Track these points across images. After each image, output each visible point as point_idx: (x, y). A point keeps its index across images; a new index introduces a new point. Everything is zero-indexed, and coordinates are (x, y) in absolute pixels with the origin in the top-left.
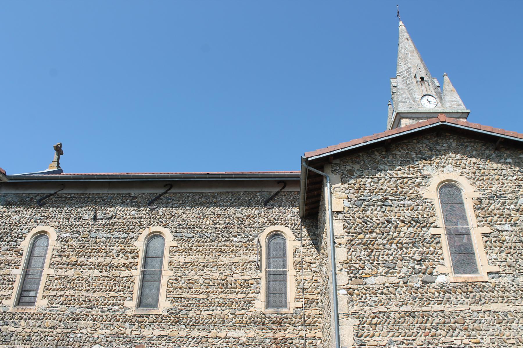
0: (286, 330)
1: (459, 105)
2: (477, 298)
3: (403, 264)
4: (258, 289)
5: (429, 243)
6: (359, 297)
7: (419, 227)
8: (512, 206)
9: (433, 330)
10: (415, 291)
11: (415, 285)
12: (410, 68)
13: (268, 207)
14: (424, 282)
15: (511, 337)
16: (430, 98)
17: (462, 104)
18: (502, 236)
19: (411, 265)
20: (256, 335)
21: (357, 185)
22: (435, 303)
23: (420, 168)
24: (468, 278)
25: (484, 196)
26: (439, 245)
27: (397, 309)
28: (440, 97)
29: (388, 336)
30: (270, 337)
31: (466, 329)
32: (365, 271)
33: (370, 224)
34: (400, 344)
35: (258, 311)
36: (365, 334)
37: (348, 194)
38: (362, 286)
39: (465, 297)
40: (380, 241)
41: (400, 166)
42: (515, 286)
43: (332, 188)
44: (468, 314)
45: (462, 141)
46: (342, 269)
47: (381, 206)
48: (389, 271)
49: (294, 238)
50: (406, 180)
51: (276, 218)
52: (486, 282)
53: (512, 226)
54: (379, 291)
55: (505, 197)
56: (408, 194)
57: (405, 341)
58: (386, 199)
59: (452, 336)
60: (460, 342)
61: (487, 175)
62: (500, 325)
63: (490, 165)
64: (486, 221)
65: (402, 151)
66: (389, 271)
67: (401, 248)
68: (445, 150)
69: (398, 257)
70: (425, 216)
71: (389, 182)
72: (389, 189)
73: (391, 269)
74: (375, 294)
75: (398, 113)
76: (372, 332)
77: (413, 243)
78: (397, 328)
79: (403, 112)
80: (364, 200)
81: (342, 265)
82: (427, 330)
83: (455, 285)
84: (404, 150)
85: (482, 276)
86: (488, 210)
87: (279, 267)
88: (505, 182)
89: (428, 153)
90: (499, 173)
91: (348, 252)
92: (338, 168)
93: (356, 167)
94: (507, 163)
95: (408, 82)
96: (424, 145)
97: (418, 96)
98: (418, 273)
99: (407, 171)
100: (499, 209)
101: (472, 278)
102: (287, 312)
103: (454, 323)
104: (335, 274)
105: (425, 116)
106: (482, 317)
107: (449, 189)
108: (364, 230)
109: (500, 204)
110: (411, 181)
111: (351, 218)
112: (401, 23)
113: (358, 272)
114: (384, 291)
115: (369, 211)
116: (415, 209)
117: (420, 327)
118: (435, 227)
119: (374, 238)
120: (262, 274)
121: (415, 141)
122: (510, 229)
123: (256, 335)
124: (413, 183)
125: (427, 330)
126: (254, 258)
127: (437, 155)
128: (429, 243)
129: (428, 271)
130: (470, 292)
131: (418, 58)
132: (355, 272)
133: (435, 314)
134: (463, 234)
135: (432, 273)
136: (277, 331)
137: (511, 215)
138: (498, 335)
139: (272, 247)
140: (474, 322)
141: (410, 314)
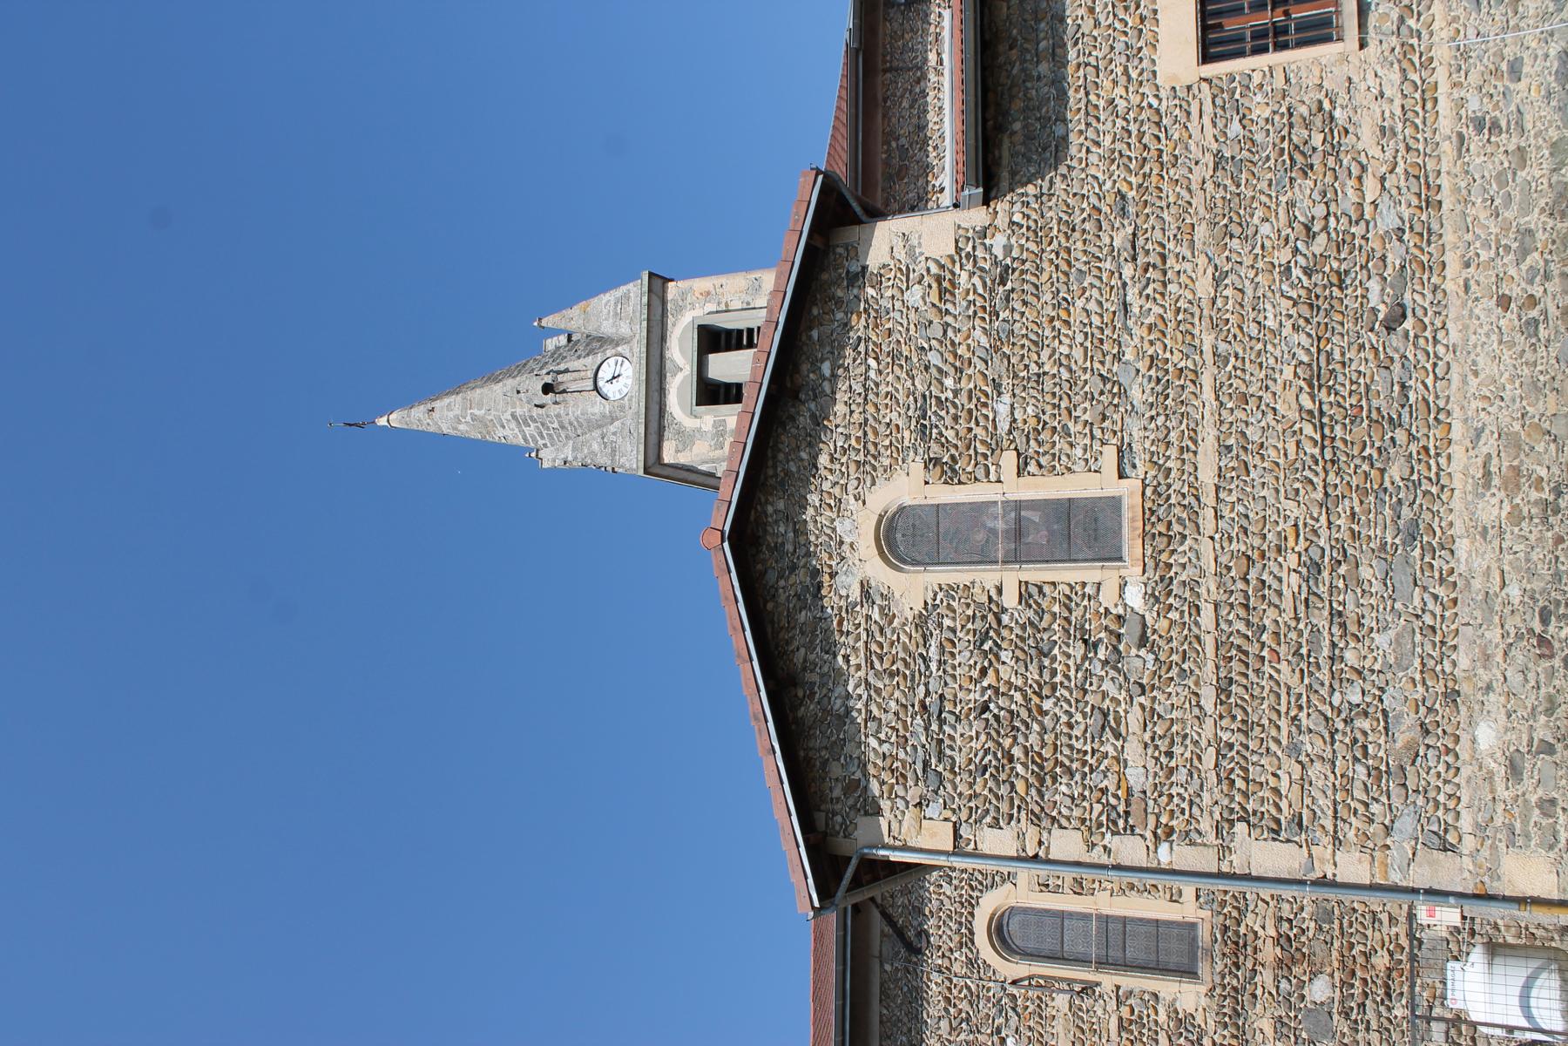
0: (1256, 933)
1: (627, 297)
2: (1185, 515)
3: (1094, 688)
4: (1146, 997)
5: (1040, 613)
6: (1177, 814)
7: (998, 634)
8: (949, 382)
9: (1264, 637)
10: (1164, 668)
11: (1150, 665)
12: (513, 416)
13: (924, 944)
14: (1143, 641)
15: (1280, 446)
16: (606, 373)
17: (623, 289)
18: (1025, 422)
19: (1098, 669)
20: (1268, 1014)
21: (885, 776)
22: (1197, 624)
23: (843, 603)
24: (1135, 529)
25: (921, 451)
26: (1047, 589)
27: (1209, 722)
28: (598, 343)
29: (1279, 753)
30: (1276, 977)
31: (1263, 556)
32: (1112, 789)
33: (989, 757)
34: (1299, 727)
35: (1204, 1002)
36: (1274, 811)
37: (907, 803)
38: (1151, 803)
39: (1182, 544)
40: (1033, 739)
41: (835, 656)
42: (1153, 413)
43: (891, 842)
44: (1225, 544)
45: (772, 481)
46: (1105, 847)
47: (942, 722)
48: (1111, 728)
49: (1008, 885)
50: (874, 647)
51: (954, 927)
52: (1145, 486)
53: (1000, 394)
54: (1163, 759)
55: (924, 396)
56: (912, 648)
57: (1292, 714)
58: (924, 706)
59: (1280, 594)
60: (1294, 577)
61: (865, 434)
62: (1251, 469)
63: (838, 421)
64: (985, 456)
65: (796, 643)
66: (1111, 728)
67: (1054, 689)
68: (795, 531)
69: (1077, 701)
70: (970, 612)
71: (878, 691)
72: (897, 694)
73: (1109, 724)
74: (1171, 771)
75: (646, 472)
76: (1266, 793)
77: (1042, 654)
78: (1257, 729)
79: (641, 457)
80: (926, 764)
81: (1094, 845)
82: (1264, 653)
83: (1150, 563)
84: (793, 637)
85: (1128, 491)
86: (956, 447)
87: (1087, 934)
88: (883, 389)
89: (801, 576)
90: (860, 400)
91: (1061, 827)
92: (839, 819)
93: (835, 770)
94: (834, 376)
95: (556, 425)
96: (782, 583)
97: (596, 407)
98: (1119, 652)
99: (851, 640)
100: (956, 418)
101: (1133, 520)
102: (1207, 926)
103: (1247, 582)
104: (1118, 867)
105: (656, 396)
106: (1232, 510)
107: (899, 536)
108: (1003, 776)
109: (943, 413)
110: (877, 634)
111: (972, 804)
112: (382, 422)
113: (1114, 808)
114: (1163, 749)
115: (956, 754)
116: (951, 636)
117: (1257, 671)
118: (1000, 591)
119: (1027, 754)
120: (1107, 981)
121: (770, 606)
122: (1006, 398)
123: (1268, 1014)
124: (882, 630)
125: (1264, 653)
126: (1061, 1001)
127: (808, 554)
128: (1040, 613)
129: (1113, 627)
130: (1169, 529)
131: (485, 390)
132: (1114, 815)
133: (1224, 626)
134: (1019, 520)
135: (1119, 617)
136: (1259, 956)
137: (970, 391)
138: (1277, 478)
139: (1031, 945)
140: (1246, 532)
141: (1223, 690)
